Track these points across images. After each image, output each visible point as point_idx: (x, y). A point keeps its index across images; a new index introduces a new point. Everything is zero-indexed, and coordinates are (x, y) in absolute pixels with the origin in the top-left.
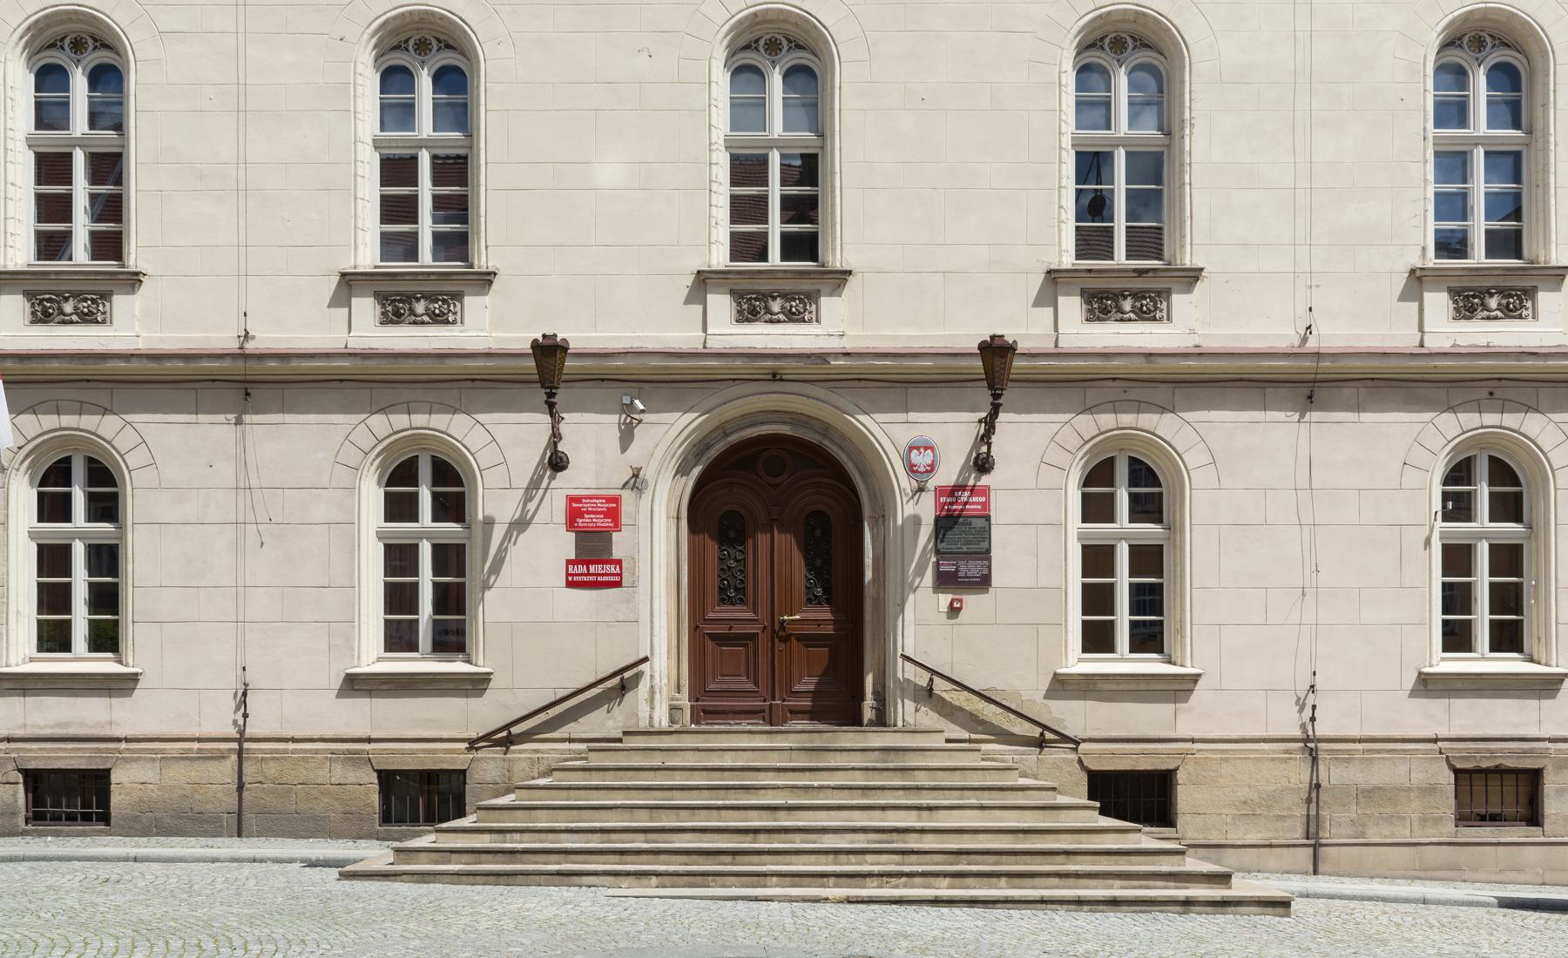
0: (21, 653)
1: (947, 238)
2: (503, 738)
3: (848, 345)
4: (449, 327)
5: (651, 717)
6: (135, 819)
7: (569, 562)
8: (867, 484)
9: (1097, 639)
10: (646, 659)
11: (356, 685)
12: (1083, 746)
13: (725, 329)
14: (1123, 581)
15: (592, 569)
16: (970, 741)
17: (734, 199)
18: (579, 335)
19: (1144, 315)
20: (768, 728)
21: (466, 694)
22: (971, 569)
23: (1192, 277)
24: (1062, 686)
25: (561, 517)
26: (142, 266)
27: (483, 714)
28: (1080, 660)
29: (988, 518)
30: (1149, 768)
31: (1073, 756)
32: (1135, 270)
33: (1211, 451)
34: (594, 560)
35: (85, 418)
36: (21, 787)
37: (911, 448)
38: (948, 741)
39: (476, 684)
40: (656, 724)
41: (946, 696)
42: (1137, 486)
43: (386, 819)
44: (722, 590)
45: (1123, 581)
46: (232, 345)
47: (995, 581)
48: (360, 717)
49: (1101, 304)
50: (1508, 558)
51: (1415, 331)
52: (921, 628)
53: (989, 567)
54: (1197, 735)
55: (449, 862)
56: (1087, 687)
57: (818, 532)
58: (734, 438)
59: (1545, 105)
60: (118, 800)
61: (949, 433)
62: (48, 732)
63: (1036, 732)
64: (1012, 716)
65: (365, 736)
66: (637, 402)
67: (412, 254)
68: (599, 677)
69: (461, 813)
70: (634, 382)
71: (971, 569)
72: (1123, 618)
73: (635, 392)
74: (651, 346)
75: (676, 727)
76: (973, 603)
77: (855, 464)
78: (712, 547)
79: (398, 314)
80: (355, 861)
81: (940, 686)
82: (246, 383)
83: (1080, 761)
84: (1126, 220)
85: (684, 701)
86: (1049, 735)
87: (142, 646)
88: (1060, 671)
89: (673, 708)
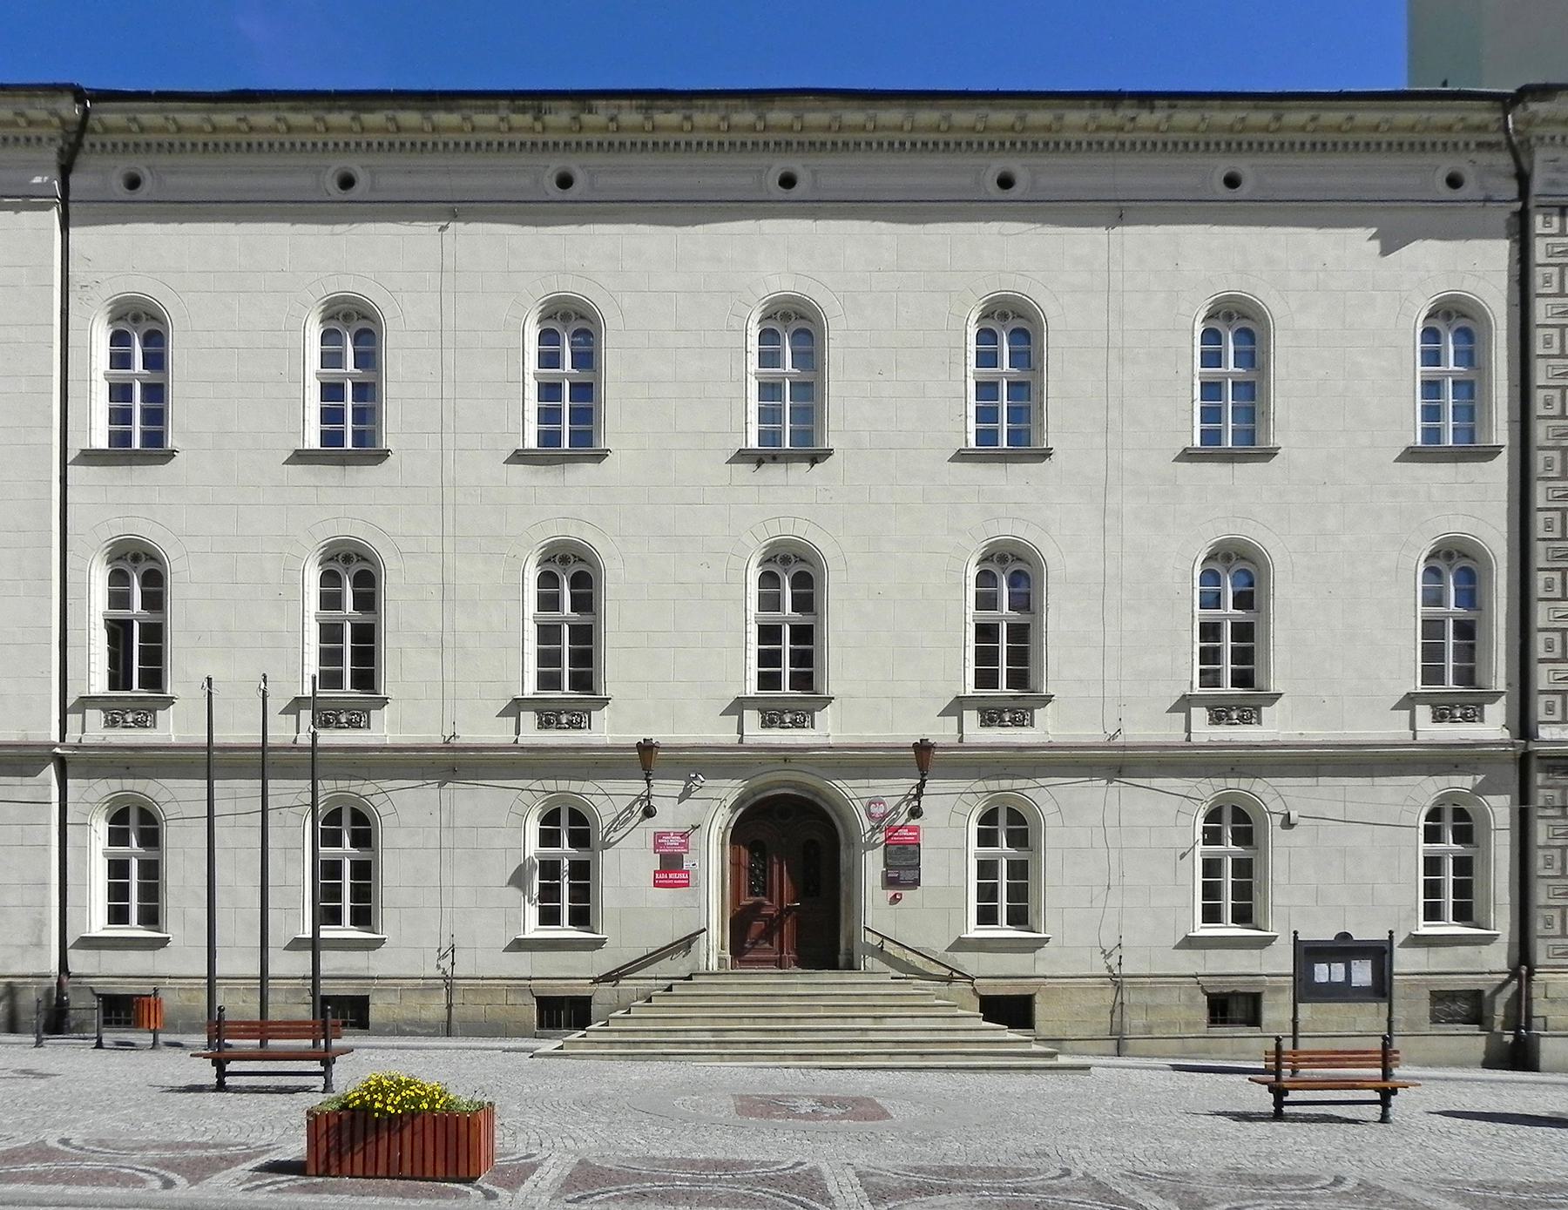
1: (894, 676)
2: (612, 977)
6: (385, 1025)
11: (520, 945)
13: (756, 732)
23: (1048, 699)
24: (961, 945)
27: (603, 962)
29: (886, 865)
33: (1058, 806)
34: (671, 868)
35: (353, 783)
39: (598, 944)
43: (541, 1025)
44: (750, 886)
46: (439, 741)
48: (522, 965)
49: (990, 717)
52: (875, 909)
59: (1268, 596)
60: (375, 1014)
61: (893, 790)
62: (335, 973)
63: (946, 972)
70: (695, 765)
71: (908, 875)
72: (1003, 904)
76: (906, 894)
78: (744, 853)
79: (549, 722)
81: (888, 946)
82: (450, 764)
84: (1008, 658)
87: (389, 922)
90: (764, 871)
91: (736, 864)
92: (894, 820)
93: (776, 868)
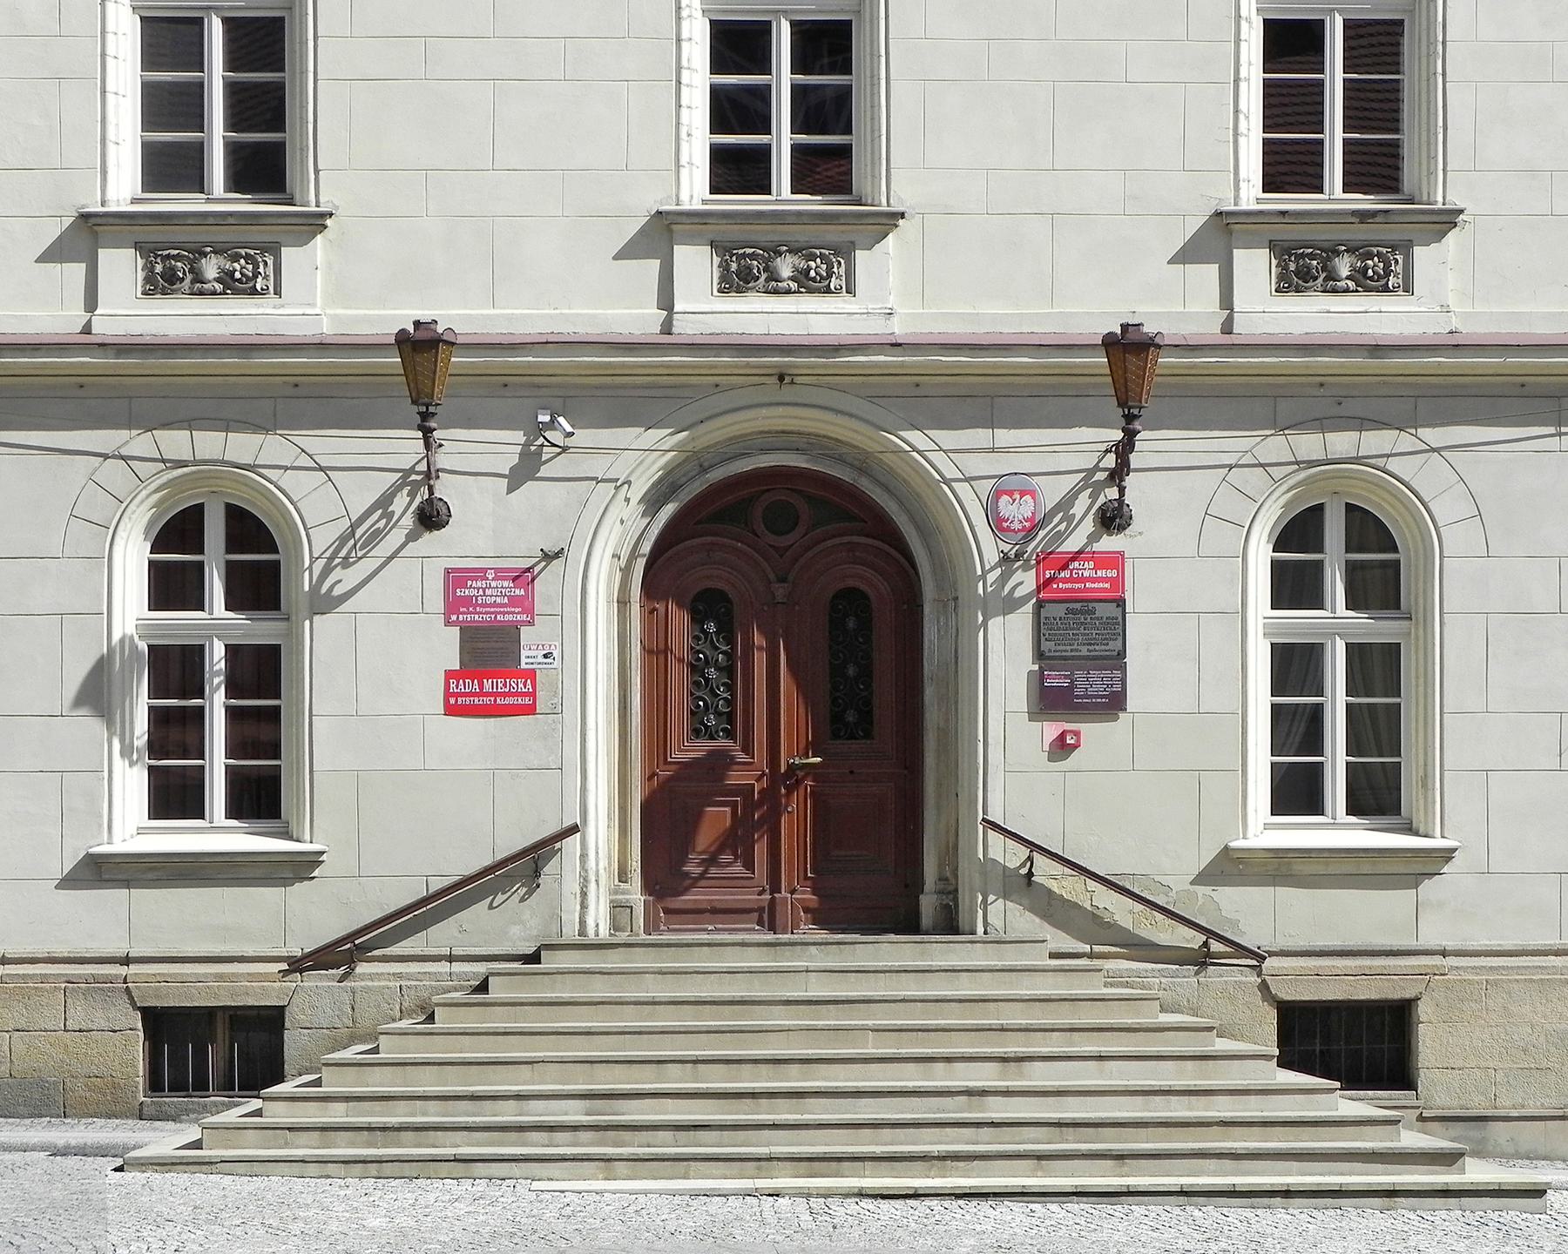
0: (131, 827)
2: (339, 955)
3: (899, 329)
4: (257, 300)
5: (583, 923)
7: (449, 675)
8: (928, 547)
9: (1296, 792)
10: (573, 829)
11: (100, 871)
12: (1270, 964)
13: (706, 306)
14: (1337, 701)
15: (487, 685)
16: (1091, 956)
17: (717, 93)
18: (457, 314)
19: (1366, 282)
20: (770, 937)
21: (285, 882)
22: (1094, 683)
23: (1447, 220)
24: (1232, 867)
25: (437, 602)
26: (1456, 200)
27: (314, 914)
28: (1267, 826)
29: (1121, 603)
30: (1374, 996)
31: (1254, 979)
32: (1354, 213)
34: (490, 667)
36: (141, 1034)
37: (998, 493)
38: (1053, 956)
39: (301, 868)
40: (591, 931)
41: (1054, 886)
42: (1361, 549)
45: (1337, 701)
47: (1131, 703)
50: (1376, 668)
51: (1214, 306)
52: (1012, 774)
53: (1124, 681)
54: (1450, 944)
55: (286, 1145)
56: (1281, 868)
57: (851, 624)
58: (716, 475)
63: (1194, 940)
64: (1159, 916)
65: (121, 953)
66: (561, 419)
67: (195, 181)
68: (500, 856)
69: (279, 1078)
70: (549, 390)
71: (1094, 683)
72: (1336, 760)
73: (558, 403)
74: (1008, 330)
75: (623, 937)
76: (1091, 732)
77: (912, 518)
78: (680, 620)
80: (135, 1148)
83: (1264, 987)
85: (635, 894)
86: (1216, 946)
88: (1233, 844)
89: (616, 906)
90: (730, 671)
91: (657, 652)
92: (1059, 537)
93: (760, 661)
